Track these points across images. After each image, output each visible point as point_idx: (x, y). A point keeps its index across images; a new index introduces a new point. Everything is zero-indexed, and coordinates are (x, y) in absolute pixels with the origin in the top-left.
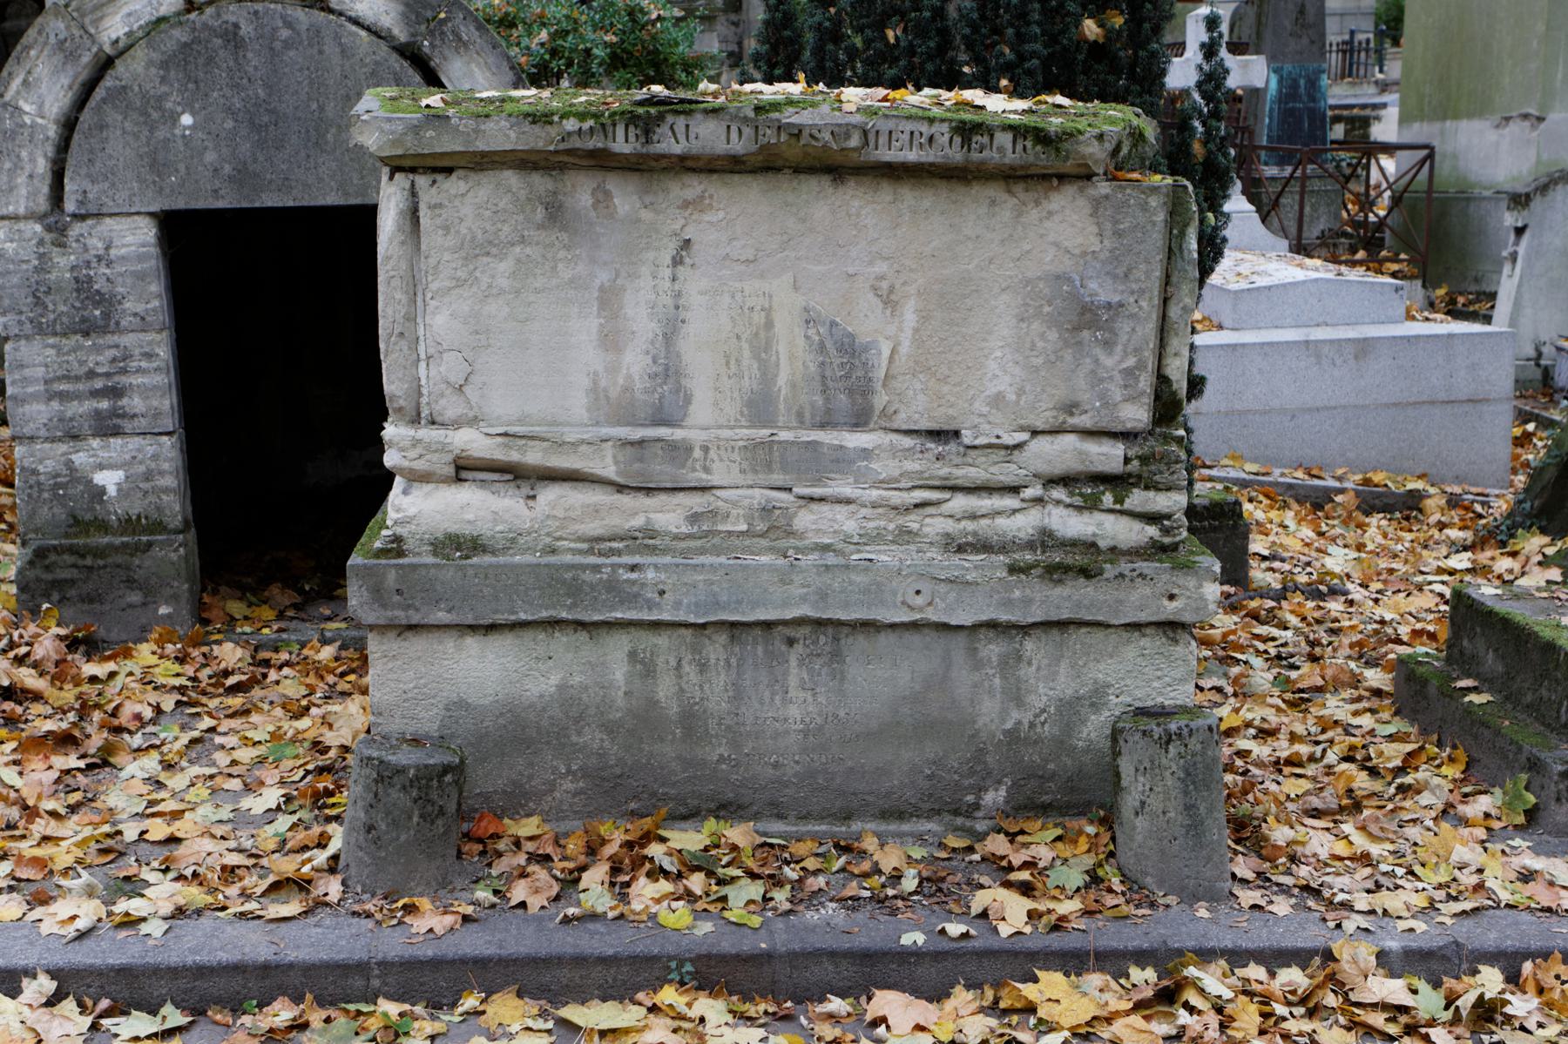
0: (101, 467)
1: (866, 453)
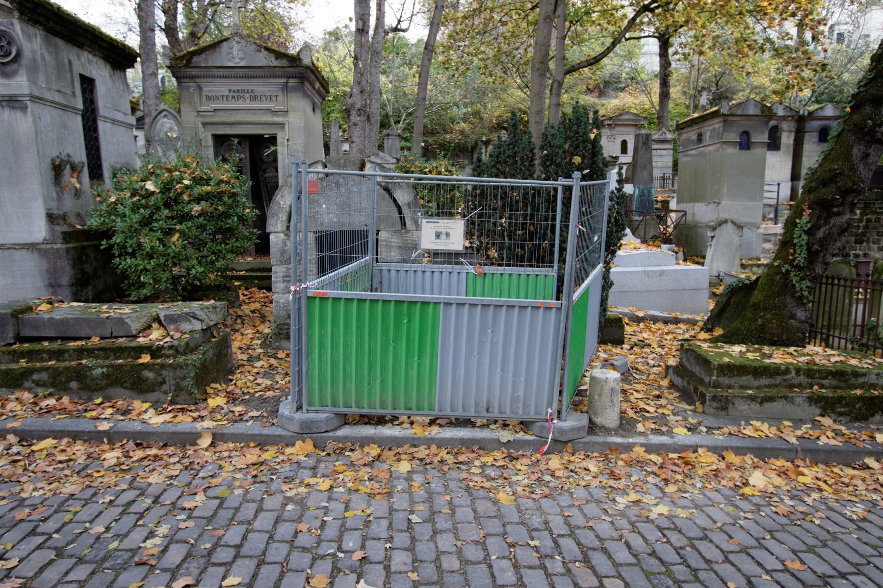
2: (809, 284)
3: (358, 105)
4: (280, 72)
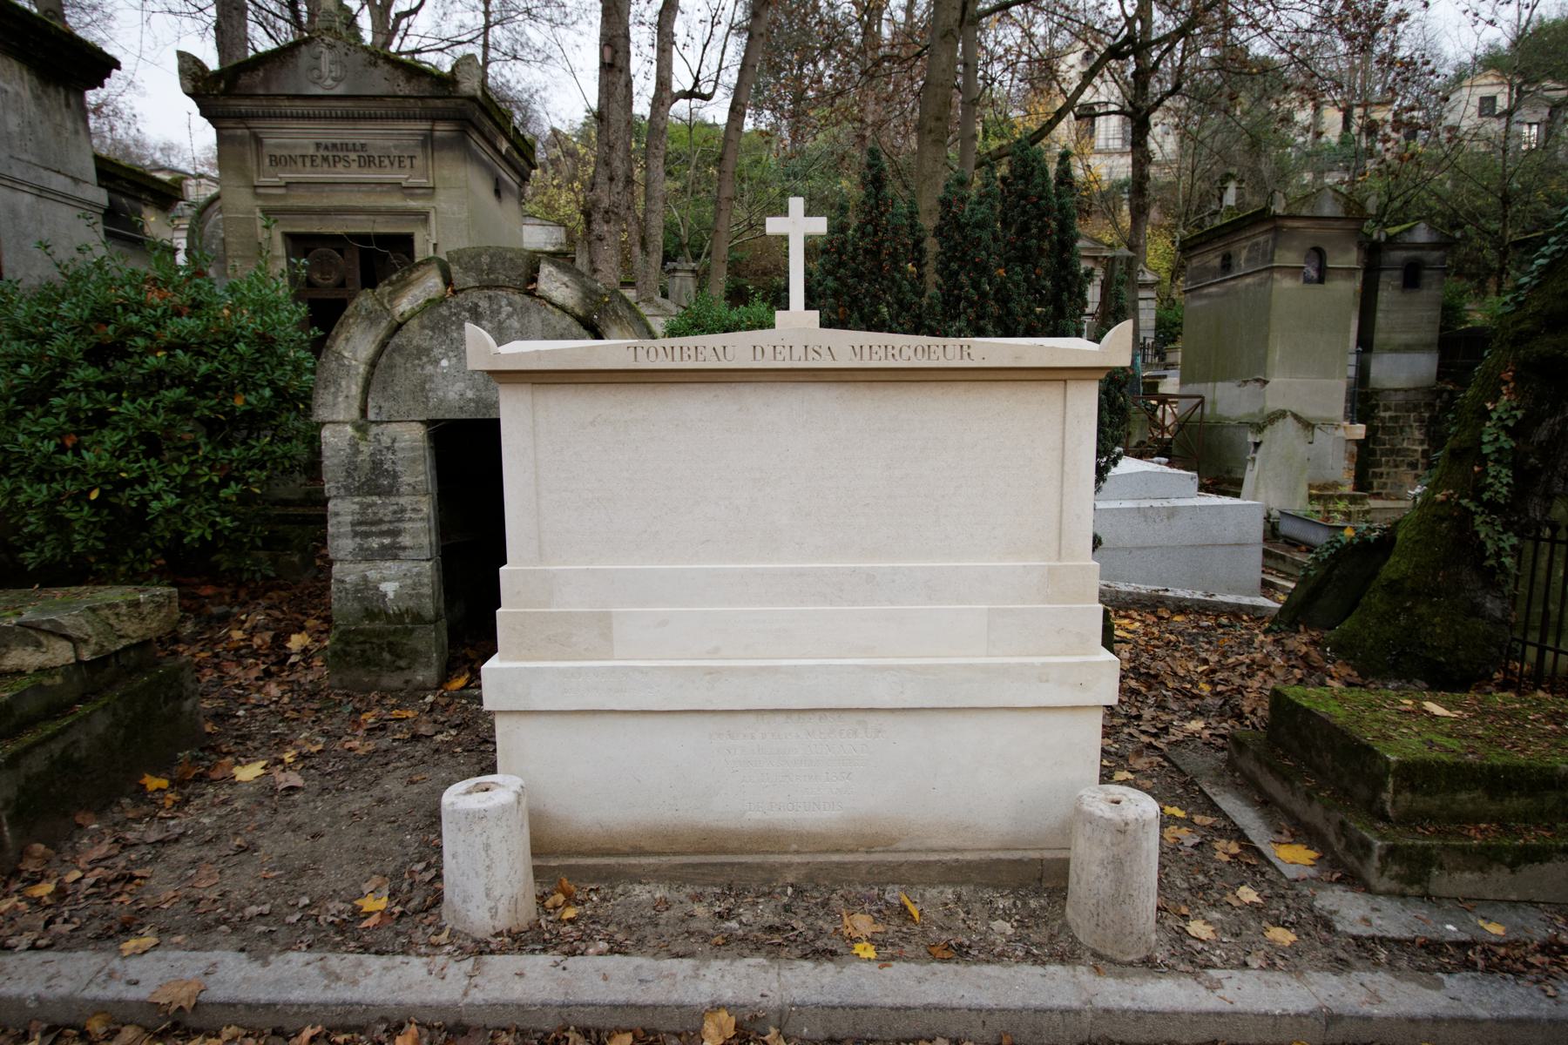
0: (384, 580)
2: (1514, 540)
3: (605, 203)
4: (416, 107)
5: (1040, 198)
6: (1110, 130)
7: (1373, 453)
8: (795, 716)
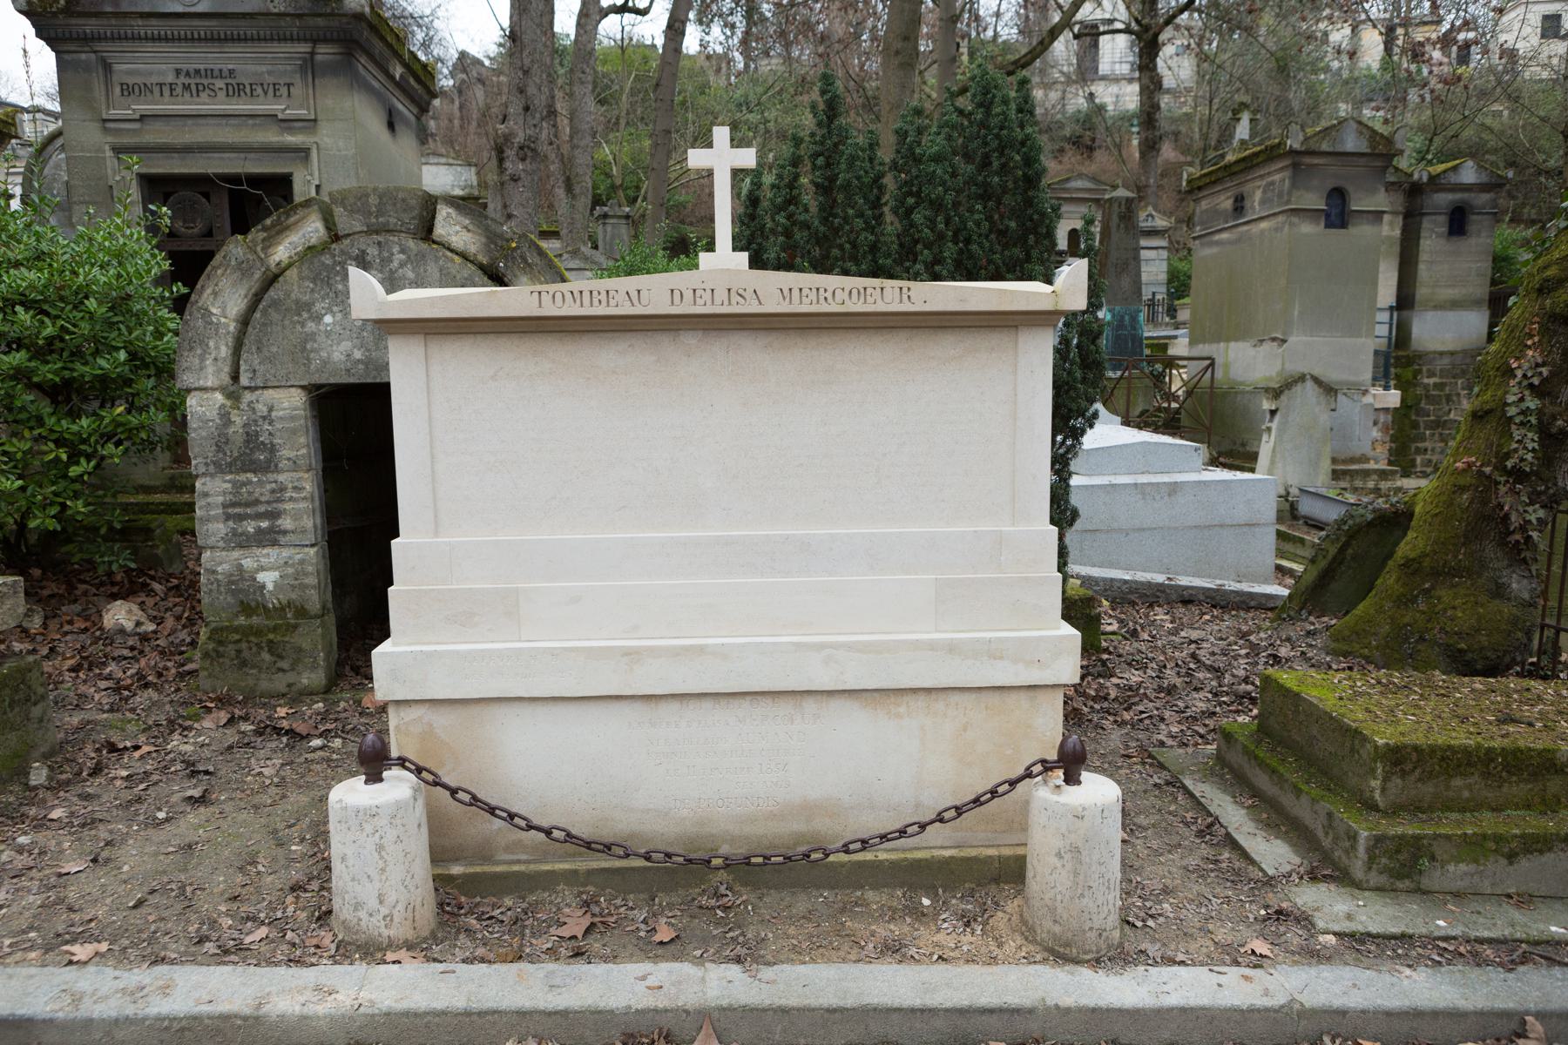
0: (262, 569)
1: (1453, 24)
2: (1541, 513)
3: (520, 138)
5: (1002, 128)
6: (1116, 52)
7: (1415, 425)
8: (723, 702)
